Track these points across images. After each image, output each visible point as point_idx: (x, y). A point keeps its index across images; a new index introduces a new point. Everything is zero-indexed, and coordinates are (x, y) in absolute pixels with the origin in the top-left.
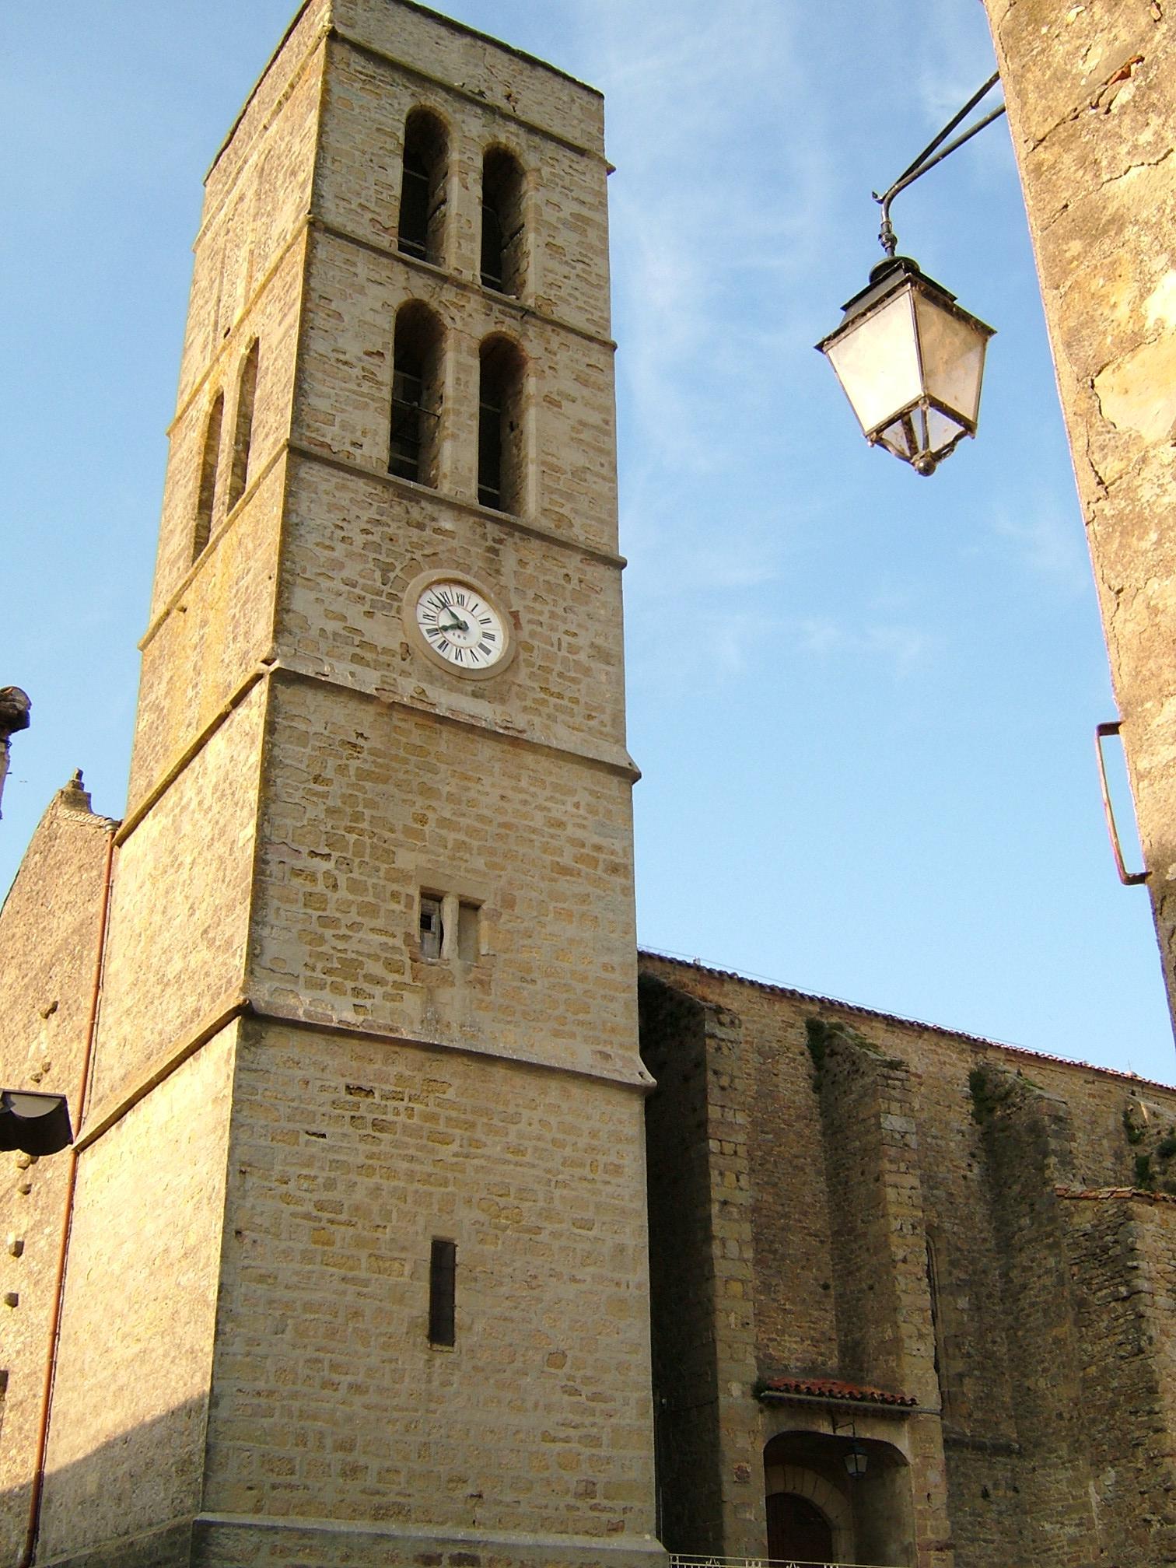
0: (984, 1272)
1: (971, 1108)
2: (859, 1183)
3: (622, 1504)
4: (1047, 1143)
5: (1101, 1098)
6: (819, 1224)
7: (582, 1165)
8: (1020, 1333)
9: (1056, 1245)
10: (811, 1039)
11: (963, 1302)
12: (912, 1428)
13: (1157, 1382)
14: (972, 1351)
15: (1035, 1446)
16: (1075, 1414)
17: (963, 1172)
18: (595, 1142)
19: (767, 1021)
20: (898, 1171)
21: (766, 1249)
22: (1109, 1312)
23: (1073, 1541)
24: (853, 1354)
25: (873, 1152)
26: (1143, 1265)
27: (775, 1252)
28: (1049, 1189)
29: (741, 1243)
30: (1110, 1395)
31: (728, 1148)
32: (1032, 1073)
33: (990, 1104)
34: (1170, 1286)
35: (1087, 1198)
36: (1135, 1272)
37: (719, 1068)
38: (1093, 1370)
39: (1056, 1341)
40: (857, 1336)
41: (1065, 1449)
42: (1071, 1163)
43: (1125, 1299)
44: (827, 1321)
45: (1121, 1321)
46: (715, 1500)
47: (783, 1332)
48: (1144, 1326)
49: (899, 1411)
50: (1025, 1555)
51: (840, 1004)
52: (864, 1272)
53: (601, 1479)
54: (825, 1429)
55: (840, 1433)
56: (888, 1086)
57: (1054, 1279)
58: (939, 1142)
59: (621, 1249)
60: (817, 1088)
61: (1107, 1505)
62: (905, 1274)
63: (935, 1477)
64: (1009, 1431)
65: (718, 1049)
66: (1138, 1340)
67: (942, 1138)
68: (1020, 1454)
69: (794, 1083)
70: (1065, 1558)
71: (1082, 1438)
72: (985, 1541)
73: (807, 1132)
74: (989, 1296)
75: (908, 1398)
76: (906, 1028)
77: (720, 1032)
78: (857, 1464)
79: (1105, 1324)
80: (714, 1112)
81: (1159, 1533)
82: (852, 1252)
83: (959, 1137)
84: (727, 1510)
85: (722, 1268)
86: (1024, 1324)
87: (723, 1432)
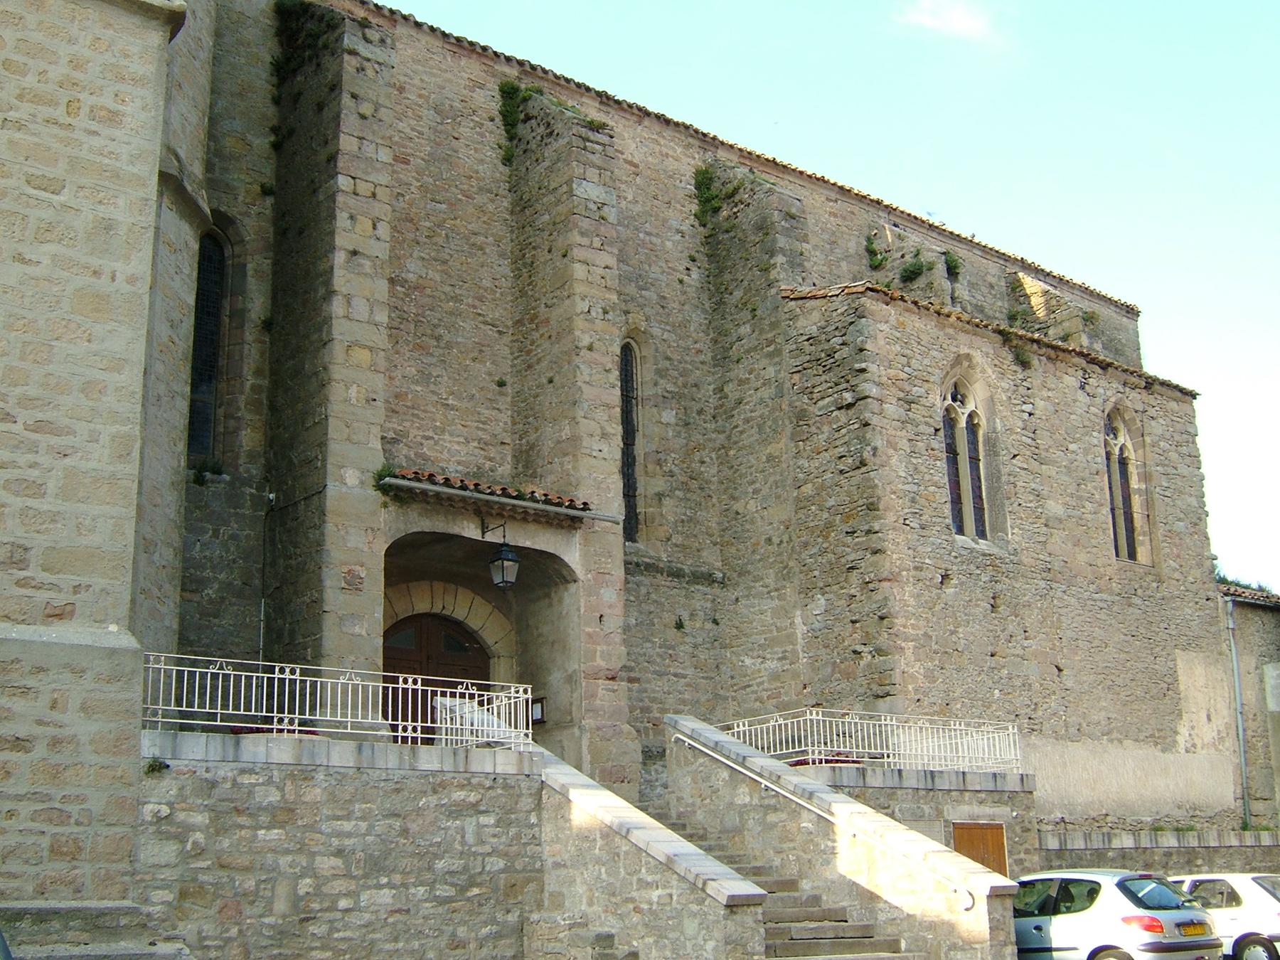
0: (696, 385)
1: (695, 207)
2: (545, 263)
3: (76, 580)
4: (774, 241)
5: (844, 218)
6: (500, 312)
7: (53, 103)
8: (732, 453)
9: (778, 352)
10: (504, 105)
11: (669, 416)
12: (586, 542)
13: (879, 498)
14: (675, 470)
15: (740, 575)
16: (786, 538)
17: (679, 276)
18: (78, 75)
19: (448, 75)
20: (591, 246)
21: (414, 323)
22: (830, 423)
23: (775, 676)
24: (526, 459)
25: (561, 225)
26: (872, 368)
27: (438, 338)
28: (773, 291)
29: (372, 303)
30: (826, 515)
31: (364, 188)
32: (770, 178)
33: (715, 203)
34: (902, 395)
35: (814, 297)
36: (862, 376)
37: (361, 92)
38: (808, 489)
39: (770, 458)
40: (533, 437)
41: (773, 576)
42: (801, 265)
43: (849, 406)
44: (501, 421)
45: (844, 431)
46: (316, 610)
47: (443, 431)
48: (868, 436)
49: (569, 518)
50: (721, 692)
51: (545, 71)
52: (544, 364)
53: (39, 542)
54: (471, 531)
55: (490, 537)
56: (585, 149)
57: (773, 390)
58: (654, 239)
59: (108, 226)
60: (507, 160)
61: (814, 636)
62: (590, 364)
63: (611, 595)
64: (711, 559)
65: (361, 69)
66: (860, 451)
67: (657, 235)
68: (723, 583)
69: (480, 149)
70: (765, 695)
71: (791, 564)
72: (675, 675)
73: (491, 207)
74: (700, 412)
75: (579, 504)
76: (623, 109)
77: (363, 49)
78: (509, 571)
79: (824, 436)
80: (347, 143)
81: (869, 665)
82: (532, 343)
83: (678, 237)
84: (329, 623)
85: (341, 330)
86: (736, 443)
87: (330, 527)
